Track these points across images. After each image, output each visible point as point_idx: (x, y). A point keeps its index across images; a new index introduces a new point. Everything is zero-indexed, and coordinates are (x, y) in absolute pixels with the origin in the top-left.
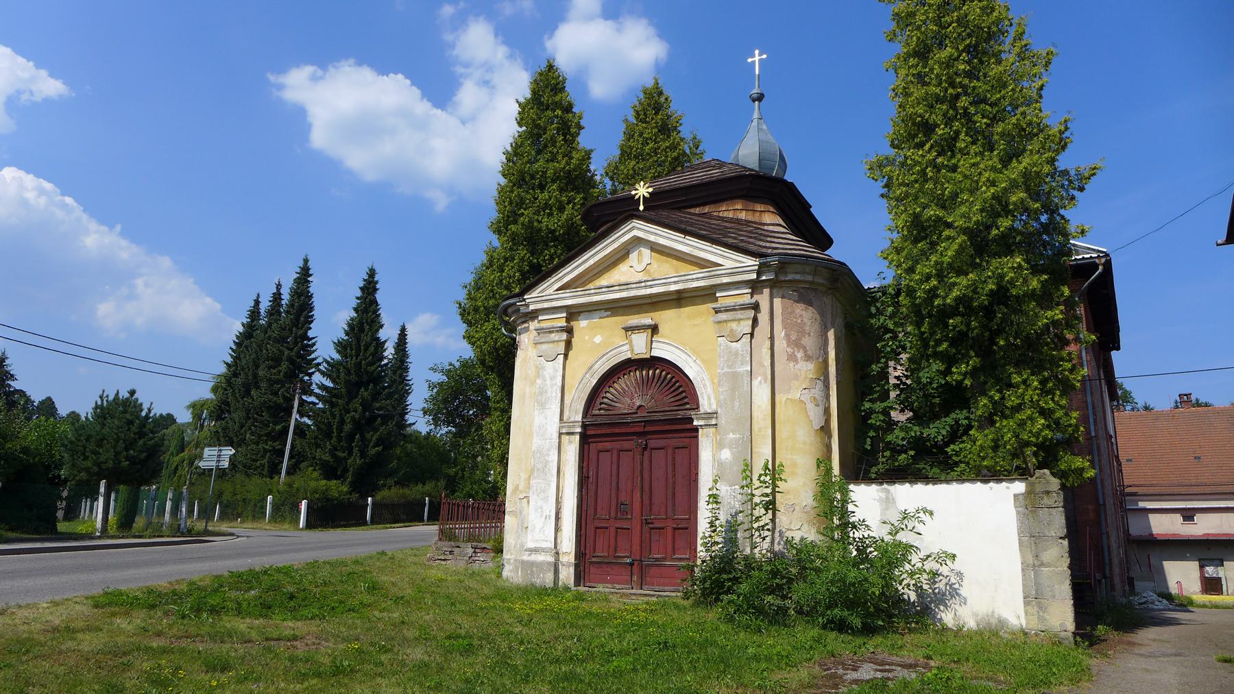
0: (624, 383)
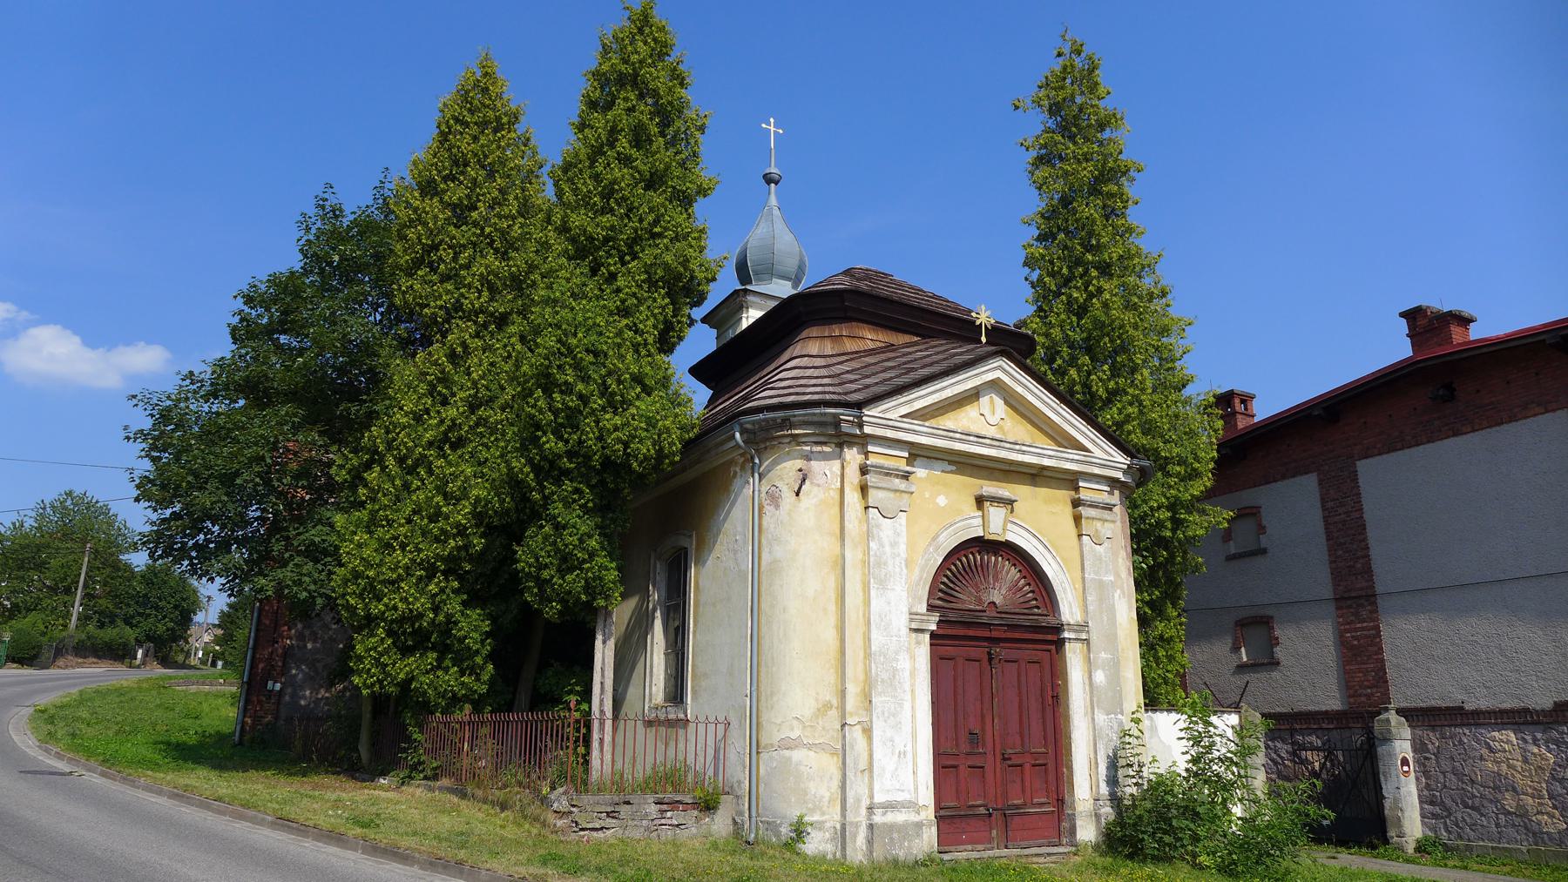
0: (1011, 573)
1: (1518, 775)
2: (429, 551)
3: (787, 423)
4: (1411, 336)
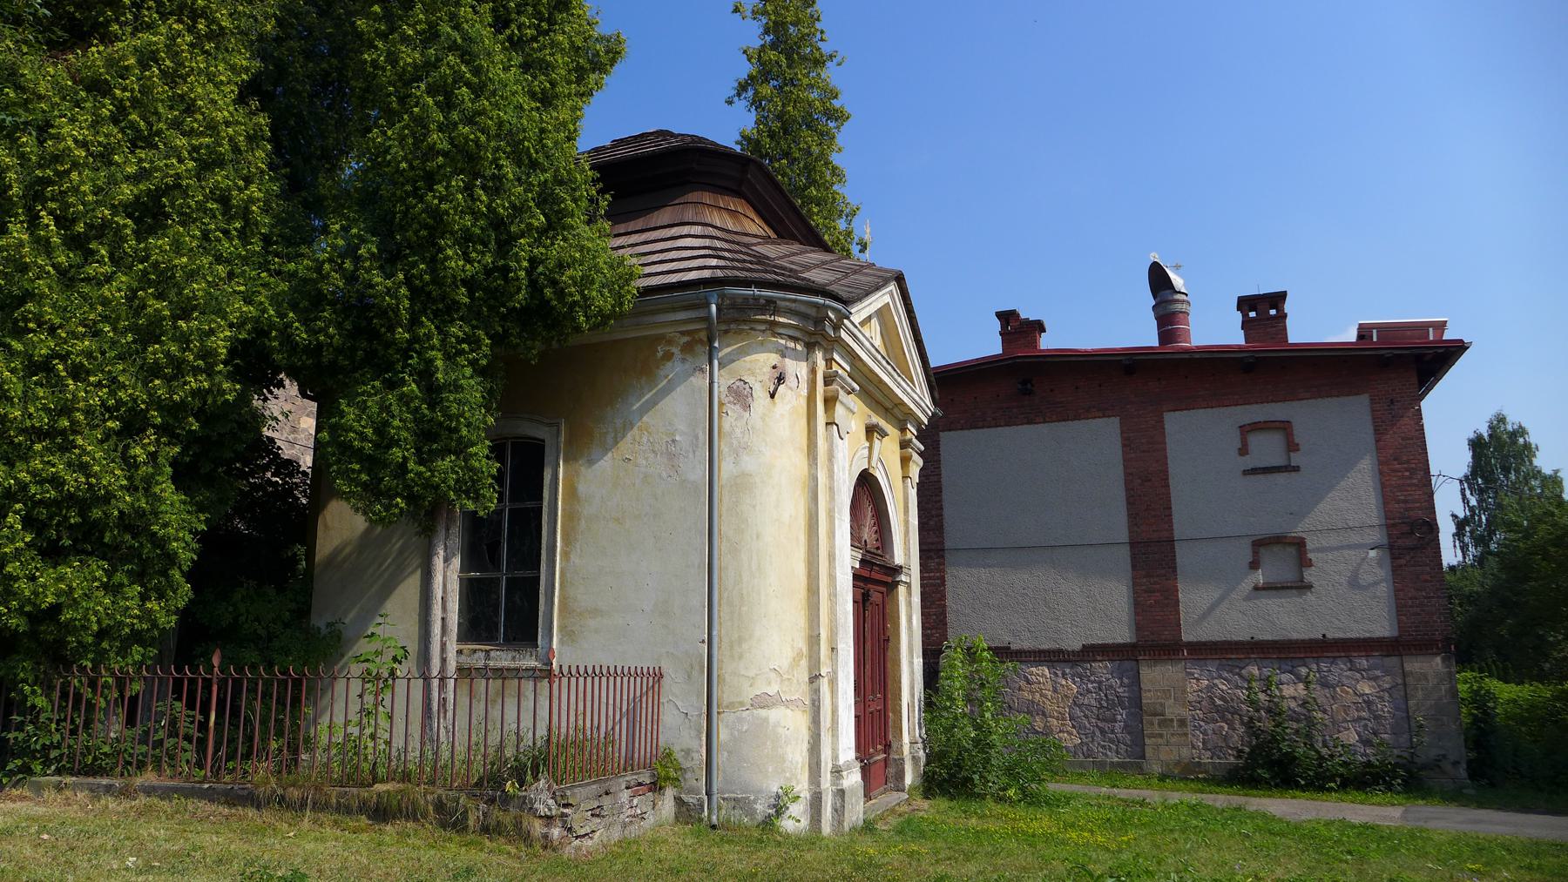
1: (1048, 703)
2: (132, 391)
3: (770, 306)
4: (1004, 334)
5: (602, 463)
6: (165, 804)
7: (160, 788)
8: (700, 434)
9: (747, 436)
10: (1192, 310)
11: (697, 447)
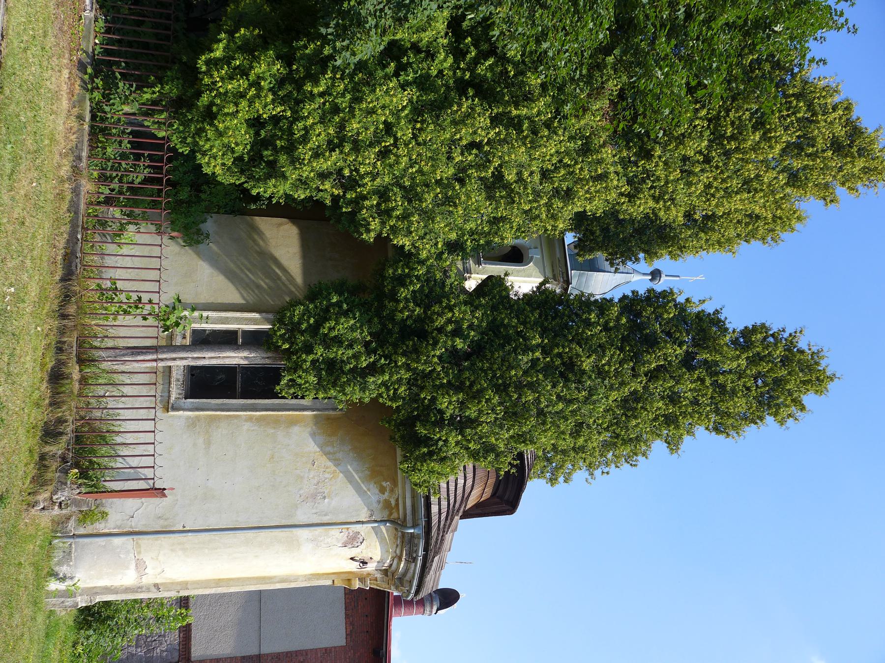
3: (412, 559)
5: (313, 444)
6: (65, 206)
7: (79, 200)
8: (328, 517)
9: (325, 546)
10: (426, 617)
11: (319, 515)
